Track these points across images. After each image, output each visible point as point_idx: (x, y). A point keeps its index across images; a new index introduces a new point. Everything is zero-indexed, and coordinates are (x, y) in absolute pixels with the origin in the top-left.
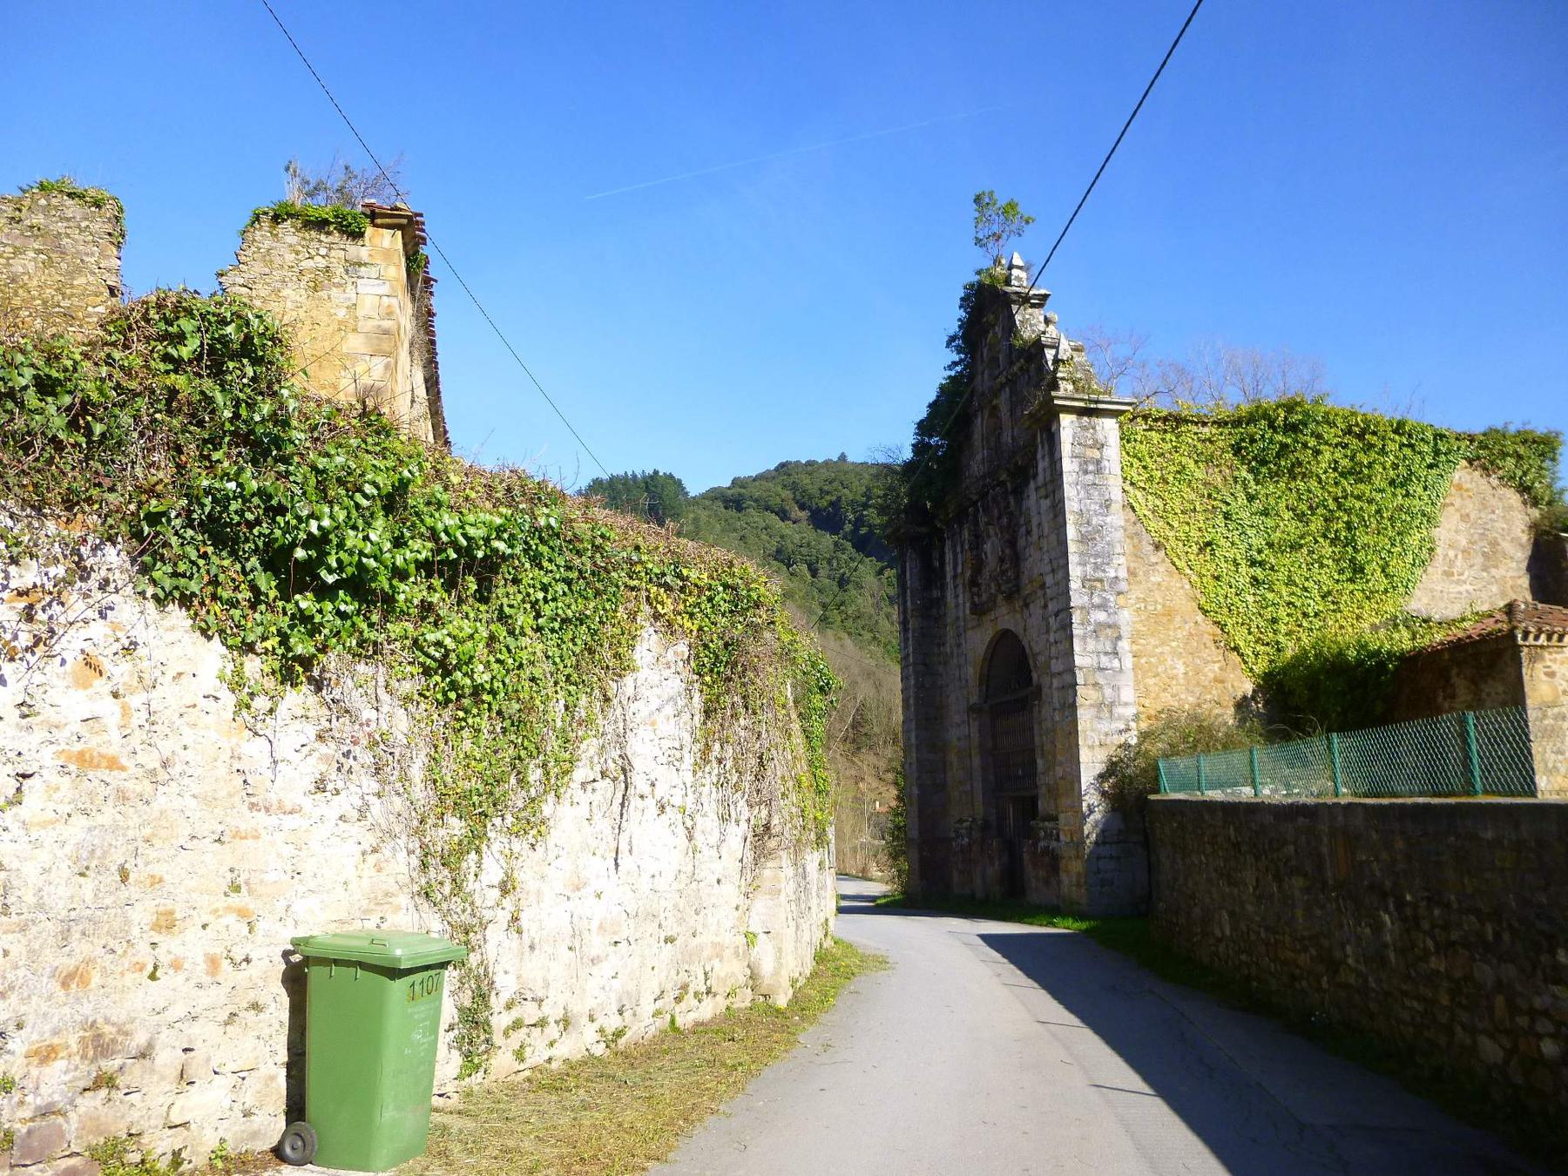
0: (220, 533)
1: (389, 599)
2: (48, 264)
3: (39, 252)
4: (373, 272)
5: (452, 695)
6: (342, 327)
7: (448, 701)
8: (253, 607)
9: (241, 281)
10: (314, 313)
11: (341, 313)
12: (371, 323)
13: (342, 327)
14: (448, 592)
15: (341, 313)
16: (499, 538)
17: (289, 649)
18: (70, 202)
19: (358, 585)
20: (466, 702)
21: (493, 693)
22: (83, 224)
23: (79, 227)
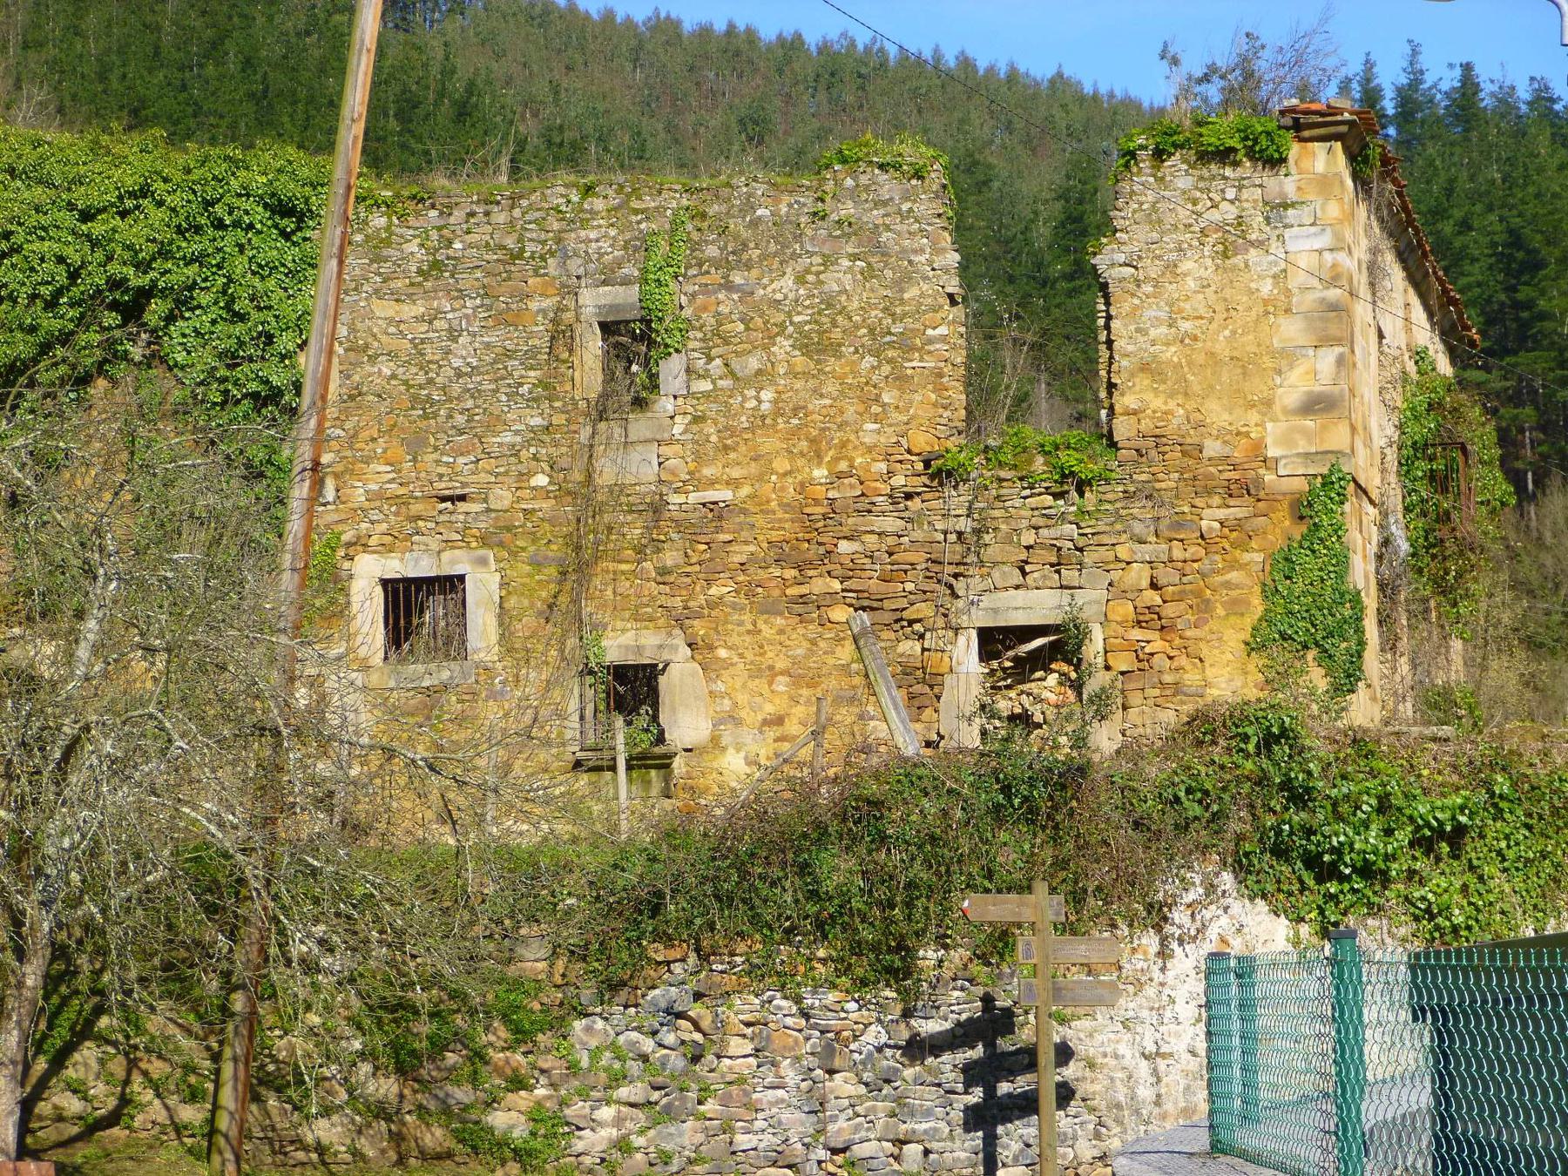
0: (1280, 852)
1: (1385, 873)
2: (869, 274)
3: (855, 257)
4: (1305, 214)
5: (1437, 935)
6: (1270, 308)
7: (1434, 939)
8: (1301, 892)
9: (1121, 258)
10: (1228, 293)
11: (1267, 287)
12: (1311, 297)
13: (1270, 308)
14: (1428, 856)
15: (1267, 287)
16: (1463, 814)
17: (1324, 917)
18: (884, 178)
19: (1365, 871)
20: (1448, 938)
21: (1469, 928)
22: (905, 207)
23: (899, 212)
